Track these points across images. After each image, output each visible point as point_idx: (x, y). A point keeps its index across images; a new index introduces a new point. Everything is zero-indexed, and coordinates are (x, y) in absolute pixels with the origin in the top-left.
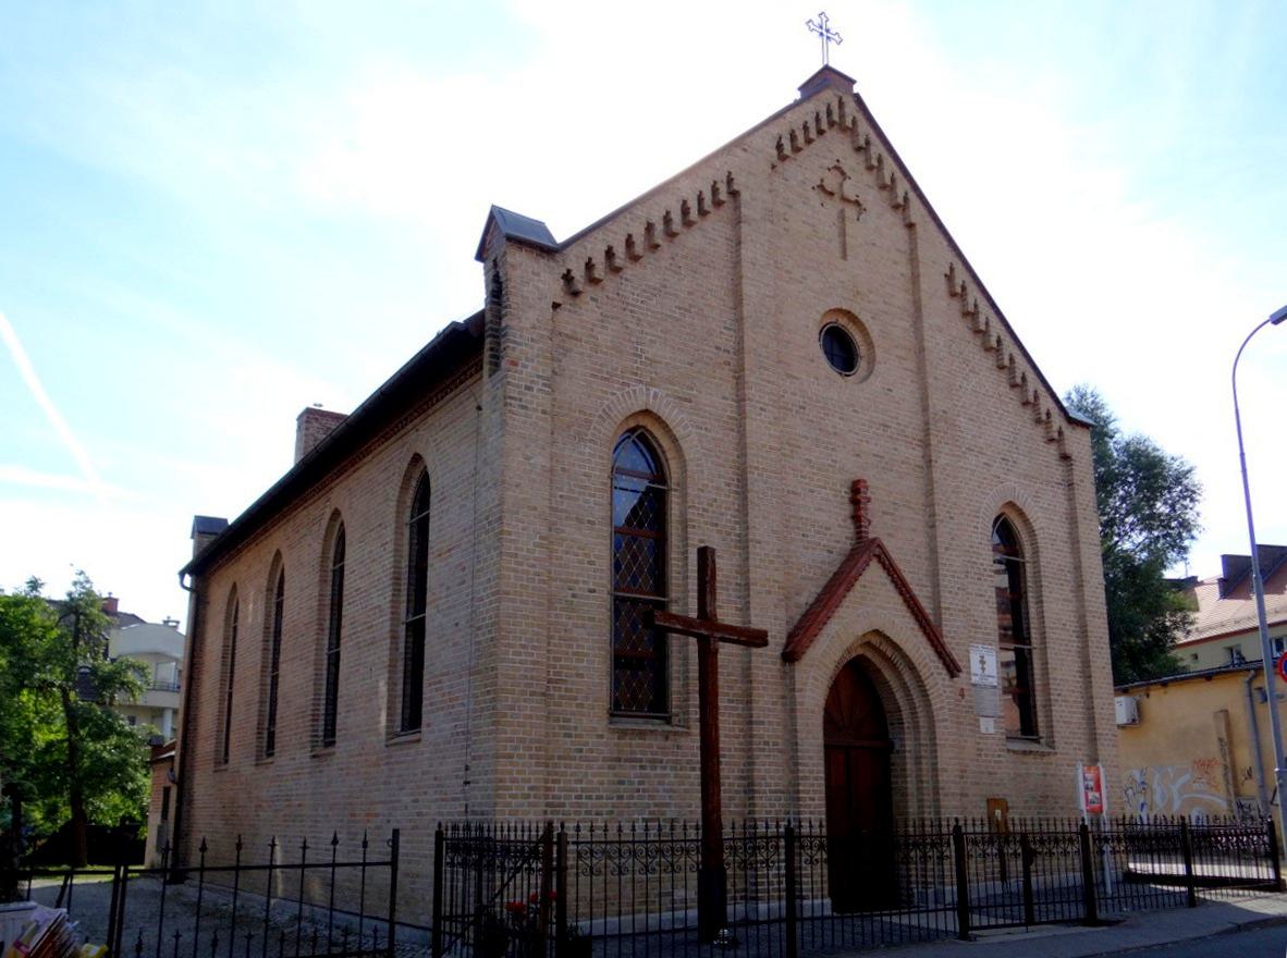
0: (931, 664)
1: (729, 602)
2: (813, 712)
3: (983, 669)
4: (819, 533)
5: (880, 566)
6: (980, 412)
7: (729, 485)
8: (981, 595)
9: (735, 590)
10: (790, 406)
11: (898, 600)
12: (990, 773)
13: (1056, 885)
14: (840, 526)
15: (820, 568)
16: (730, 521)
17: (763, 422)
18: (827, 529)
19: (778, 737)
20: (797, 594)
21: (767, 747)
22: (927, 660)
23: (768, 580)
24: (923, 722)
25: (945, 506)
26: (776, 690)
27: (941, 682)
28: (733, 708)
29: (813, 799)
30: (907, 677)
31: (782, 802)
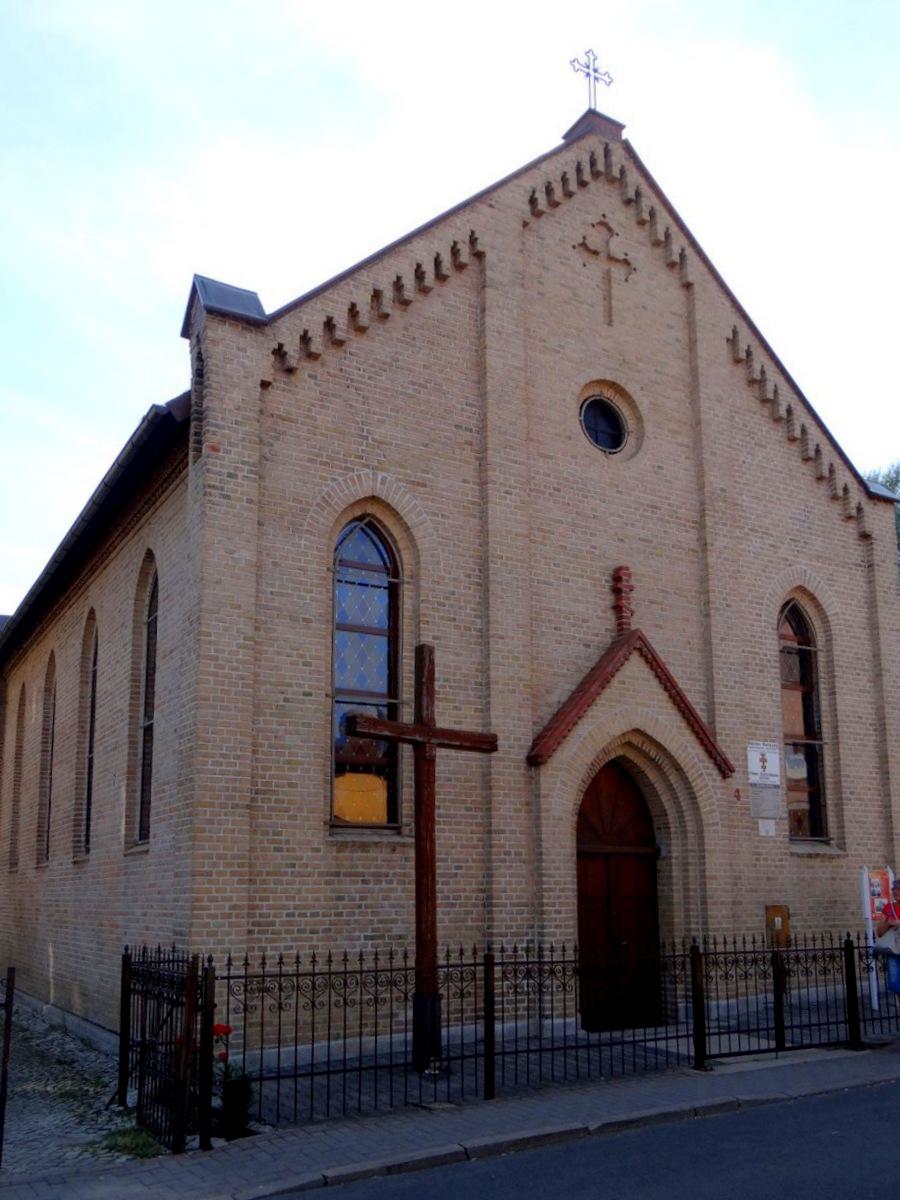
0: (700, 765)
1: (469, 703)
3: (764, 767)
7: (469, 576)
8: (763, 688)
12: (769, 879)
18: (584, 621)
20: (547, 692)
21: (507, 857)
22: (696, 760)
23: (511, 678)
24: (690, 825)
28: (474, 817)
30: (673, 778)
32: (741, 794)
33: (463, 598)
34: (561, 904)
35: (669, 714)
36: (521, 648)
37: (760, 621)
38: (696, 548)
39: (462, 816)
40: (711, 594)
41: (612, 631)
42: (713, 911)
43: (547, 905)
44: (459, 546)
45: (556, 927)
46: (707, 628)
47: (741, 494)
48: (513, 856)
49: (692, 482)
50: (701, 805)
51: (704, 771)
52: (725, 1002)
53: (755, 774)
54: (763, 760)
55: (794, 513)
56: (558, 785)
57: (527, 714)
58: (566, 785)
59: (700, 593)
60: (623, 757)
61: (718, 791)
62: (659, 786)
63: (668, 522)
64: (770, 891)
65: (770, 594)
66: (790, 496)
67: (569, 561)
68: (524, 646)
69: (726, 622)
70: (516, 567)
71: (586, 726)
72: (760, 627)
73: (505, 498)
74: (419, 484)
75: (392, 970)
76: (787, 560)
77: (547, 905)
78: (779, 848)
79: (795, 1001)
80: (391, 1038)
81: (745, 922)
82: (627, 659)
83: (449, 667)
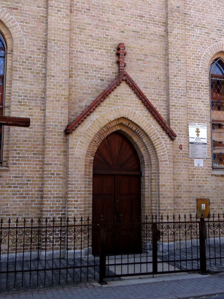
0: (158, 133)
1: (37, 106)
2: (79, 158)
3: (198, 135)
4: (95, 71)
5: (128, 86)
6: (204, 7)
7: (39, 49)
8: (199, 99)
9: (39, 100)
10: (80, 9)
11: (139, 102)
12: (199, 186)
13: (183, 247)
14: (109, 67)
15: (95, 88)
16: (39, 67)
17: (59, 17)
18: (101, 69)
19: (60, 171)
20: (80, 101)
21: (52, 176)
22: (156, 131)
23: (57, 95)
24: (153, 161)
25: (175, 54)
26: (60, 148)
27: (163, 142)
28: (37, 158)
29: (77, 201)
30: (145, 140)
31: (61, 202)
32: (183, 147)
33: (35, 59)
34: (78, 197)
35: (141, 110)
36: (64, 81)
37: (199, 68)
38: (164, 35)
39: (31, 157)
40: (170, 56)
41: (116, 73)
42: (162, 201)
43: (70, 197)
44: (35, 36)
45: (75, 208)
46: (167, 70)
47: (190, 10)
48: (55, 176)
49: (163, 5)
50: (158, 152)
51: (160, 136)
52: (167, 244)
53: (193, 138)
54: (198, 131)
55: (220, 18)
56: (79, 143)
57: (66, 111)
58: (83, 143)
59: (165, 55)
60: (120, 130)
61: (168, 146)
62: (139, 144)
63: (149, 23)
64: (200, 192)
65: (204, 55)
66: (218, 10)
67: (94, 42)
68: (65, 80)
69: (178, 68)
70: (62, 44)
71: (95, 116)
72: (199, 70)
73: (58, 13)
74: (14, 9)
75: (9, 228)
76: (215, 39)
77: (70, 197)
78: (205, 172)
79: (212, 243)
80: (16, 255)
81: (183, 206)
82: (118, 85)
83: (27, 90)
